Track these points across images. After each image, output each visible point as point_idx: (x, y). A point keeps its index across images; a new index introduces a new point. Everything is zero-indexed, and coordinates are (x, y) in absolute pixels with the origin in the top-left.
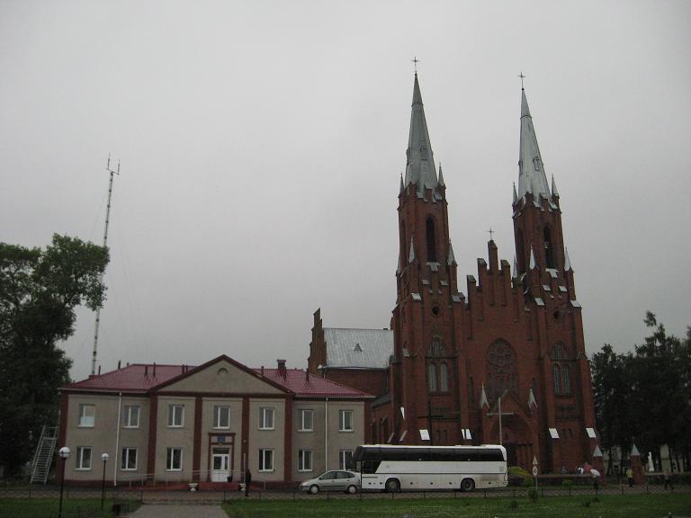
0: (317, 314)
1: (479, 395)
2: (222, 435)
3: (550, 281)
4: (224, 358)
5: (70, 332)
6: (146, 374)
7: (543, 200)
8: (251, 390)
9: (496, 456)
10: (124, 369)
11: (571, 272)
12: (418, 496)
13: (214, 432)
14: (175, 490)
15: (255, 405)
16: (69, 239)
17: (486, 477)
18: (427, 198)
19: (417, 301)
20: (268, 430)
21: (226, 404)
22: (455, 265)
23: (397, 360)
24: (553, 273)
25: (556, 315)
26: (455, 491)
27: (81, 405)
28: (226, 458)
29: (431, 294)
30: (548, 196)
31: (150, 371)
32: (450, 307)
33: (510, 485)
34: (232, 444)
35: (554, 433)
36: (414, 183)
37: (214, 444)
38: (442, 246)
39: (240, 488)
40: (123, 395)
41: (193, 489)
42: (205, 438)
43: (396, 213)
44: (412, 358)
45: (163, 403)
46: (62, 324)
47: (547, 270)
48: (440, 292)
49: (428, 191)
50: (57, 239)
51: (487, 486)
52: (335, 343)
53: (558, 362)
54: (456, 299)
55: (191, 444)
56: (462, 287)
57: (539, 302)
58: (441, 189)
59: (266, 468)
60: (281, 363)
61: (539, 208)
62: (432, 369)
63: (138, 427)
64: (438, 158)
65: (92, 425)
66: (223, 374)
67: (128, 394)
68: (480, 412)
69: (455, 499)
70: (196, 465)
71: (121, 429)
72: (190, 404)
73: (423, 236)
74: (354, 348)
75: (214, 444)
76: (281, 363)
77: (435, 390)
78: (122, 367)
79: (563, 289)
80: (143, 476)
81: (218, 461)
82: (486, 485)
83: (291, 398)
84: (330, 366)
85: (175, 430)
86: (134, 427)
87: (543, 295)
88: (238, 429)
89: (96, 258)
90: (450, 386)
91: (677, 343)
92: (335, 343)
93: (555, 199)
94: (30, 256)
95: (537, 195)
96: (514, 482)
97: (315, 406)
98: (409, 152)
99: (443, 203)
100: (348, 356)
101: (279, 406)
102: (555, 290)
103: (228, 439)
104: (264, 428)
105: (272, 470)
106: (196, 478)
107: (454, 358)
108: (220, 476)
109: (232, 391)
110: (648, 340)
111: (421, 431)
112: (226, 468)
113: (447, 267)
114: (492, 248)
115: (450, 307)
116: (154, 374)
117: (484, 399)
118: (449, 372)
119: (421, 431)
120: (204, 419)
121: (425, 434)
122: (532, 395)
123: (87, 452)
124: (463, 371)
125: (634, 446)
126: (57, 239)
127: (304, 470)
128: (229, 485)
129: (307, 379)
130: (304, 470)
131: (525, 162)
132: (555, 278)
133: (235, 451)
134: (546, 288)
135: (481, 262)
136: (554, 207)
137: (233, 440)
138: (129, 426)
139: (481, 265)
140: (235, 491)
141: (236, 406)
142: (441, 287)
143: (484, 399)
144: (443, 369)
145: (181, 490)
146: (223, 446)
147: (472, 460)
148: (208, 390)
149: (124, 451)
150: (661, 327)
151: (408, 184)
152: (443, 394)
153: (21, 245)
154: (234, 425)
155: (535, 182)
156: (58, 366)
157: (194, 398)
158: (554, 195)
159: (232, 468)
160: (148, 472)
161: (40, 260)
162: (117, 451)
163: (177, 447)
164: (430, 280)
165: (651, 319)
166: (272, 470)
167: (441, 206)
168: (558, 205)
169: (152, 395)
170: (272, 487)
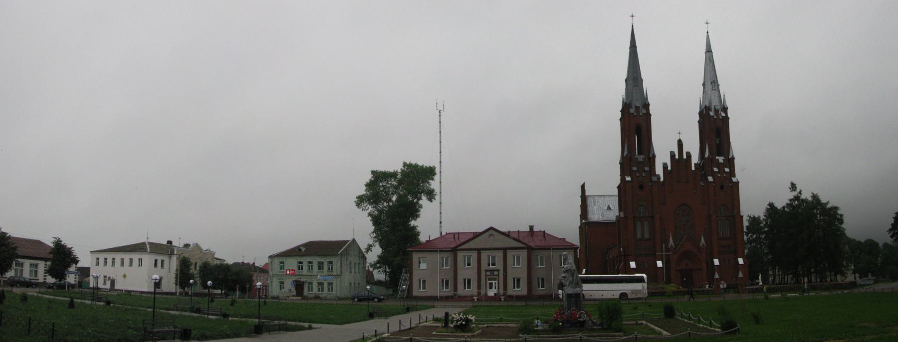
0: (583, 186)
2: (492, 271)
4: (491, 228)
5: (418, 216)
8: (507, 246)
9: (640, 280)
10: (444, 236)
11: (733, 158)
12: (592, 302)
14: (467, 301)
15: (510, 254)
16: (412, 164)
17: (634, 292)
18: (637, 113)
19: (628, 181)
20: (518, 268)
21: (494, 254)
22: (654, 156)
24: (721, 159)
25: (722, 187)
26: (645, 299)
27: (419, 258)
28: (495, 283)
29: (638, 176)
30: (718, 108)
31: (456, 236)
33: (648, 296)
34: (498, 275)
35: (716, 262)
36: (628, 103)
37: (488, 276)
39: (501, 299)
40: (440, 251)
41: (476, 300)
42: (483, 273)
43: (619, 122)
45: (460, 255)
46: (413, 211)
47: (717, 158)
49: (637, 108)
50: (405, 164)
51: (636, 297)
52: (594, 205)
53: (721, 218)
54: (654, 179)
55: (476, 276)
57: (710, 179)
58: (647, 106)
59: (517, 288)
60: (531, 228)
61: (713, 116)
64: (646, 85)
65: (425, 268)
66: (492, 237)
67: (442, 251)
69: (508, 305)
70: (479, 287)
71: (440, 269)
72: (474, 255)
74: (606, 208)
75: (488, 276)
76: (531, 228)
78: (443, 235)
79: (727, 170)
80: (452, 293)
81: (491, 284)
82: (634, 296)
83: (530, 249)
84: (591, 220)
85: (467, 272)
87: (713, 174)
89: (429, 173)
92: (594, 205)
93: (725, 109)
94: (393, 175)
96: (651, 294)
97: (546, 253)
98: (626, 81)
99: (648, 116)
100: (602, 213)
101: (524, 254)
102: (721, 170)
103: (496, 273)
104: (516, 266)
105: (520, 289)
106: (479, 294)
108: (491, 293)
112: (495, 288)
113: (649, 158)
115: (650, 184)
116: (458, 238)
120: (502, 259)
121: (633, 265)
122: (702, 238)
123: (424, 282)
125: (740, 272)
126: (405, 164)
127: (541, 289)
128: (496, 297)
130: (541, 289)
131: (706, 84)
132: (722, 163)
134: (716, 170)
136: (723, 115)
137: (486, 273)
138: (445, 268)
139: (672, 155)
140: (497, 301)
141: (499, 255)
142: (644, 171)
144: (646, 224)
145: (470, 301)
146: (493, 277)
147: (626, 283)
148: (484, 247)
149: (443, 281)
153: (386, 170)
154: (499, 265)
155: (713, 97)
156: (413, 234)
159: (499, 288)
160: (454, 291)
161: (399, 176)
162: (439, 280)
163: (469, 278)
165: (793, 187)
166: (520, 289)
169: (454, 250)
170: (519, 298)
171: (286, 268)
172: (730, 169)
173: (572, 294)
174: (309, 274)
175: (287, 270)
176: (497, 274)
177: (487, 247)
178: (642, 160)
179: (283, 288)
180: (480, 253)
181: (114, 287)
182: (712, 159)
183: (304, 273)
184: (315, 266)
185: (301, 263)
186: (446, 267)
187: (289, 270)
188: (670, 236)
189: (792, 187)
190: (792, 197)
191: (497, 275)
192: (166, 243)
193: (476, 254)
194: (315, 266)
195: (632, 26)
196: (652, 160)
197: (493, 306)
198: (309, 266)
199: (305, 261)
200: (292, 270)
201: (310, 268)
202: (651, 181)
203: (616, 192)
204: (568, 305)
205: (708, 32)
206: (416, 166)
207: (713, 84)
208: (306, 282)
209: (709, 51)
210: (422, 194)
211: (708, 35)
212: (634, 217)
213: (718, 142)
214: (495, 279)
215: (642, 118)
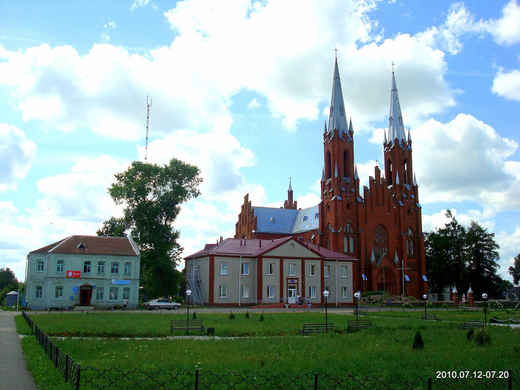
0: (246, 197)
1: (370, 255)
2: (292, 279)
6: (241, 244)
13: (289, 277)
24: (408, 187)
25: (409, 211)
28: (294, 291)
34: (297, 283)
40: (243, 257)
42: (285, 281)
45: (266, 263)
48: (351, 196)
54: (360, 200)
56: (361, 193)
63: (248, 274)
72: (277, 262)
81: (291, 292)
86: (247, 274)
88: (299, 276)
90: (354, 249)
91: (463, 229)
95: (400, 140)
101: (318, 263)
103: (296, 281)
109: (297, 256)
110: (447, 225)
112: (294, 296)
116: (245, 245)
117: (373, 258)
118: (354, 242)
124: (363, 242)
129: (319, 249)
142: (351, 192)
143: (373, 258)
144: (351, 239)
151: (331, 129)
157: (279, 259)
163: (345, 286)
164: (346, 188)
171: (65, 270)
174: (98, 277)
175: (68, 272)
177: (288, 256)
179: (61, 295)
180: (304, 261)
181: (319, 304)
183: (92, 277)
184: (108, 268)
185: (116, 264)
186: (245, 273)
187: (72, 272)
191: (296, 283)
192: (96, 235)
193: (352, 265)
194: (108, 268)
196: (356, 182)
198: (99, 268)
199: (94, 261)
200: (76, 272)
201: (101, 270)
206: (498, 192)
207: (400, 119)
208: (95, 286)
210: (123, 184)
214: (294, 288)
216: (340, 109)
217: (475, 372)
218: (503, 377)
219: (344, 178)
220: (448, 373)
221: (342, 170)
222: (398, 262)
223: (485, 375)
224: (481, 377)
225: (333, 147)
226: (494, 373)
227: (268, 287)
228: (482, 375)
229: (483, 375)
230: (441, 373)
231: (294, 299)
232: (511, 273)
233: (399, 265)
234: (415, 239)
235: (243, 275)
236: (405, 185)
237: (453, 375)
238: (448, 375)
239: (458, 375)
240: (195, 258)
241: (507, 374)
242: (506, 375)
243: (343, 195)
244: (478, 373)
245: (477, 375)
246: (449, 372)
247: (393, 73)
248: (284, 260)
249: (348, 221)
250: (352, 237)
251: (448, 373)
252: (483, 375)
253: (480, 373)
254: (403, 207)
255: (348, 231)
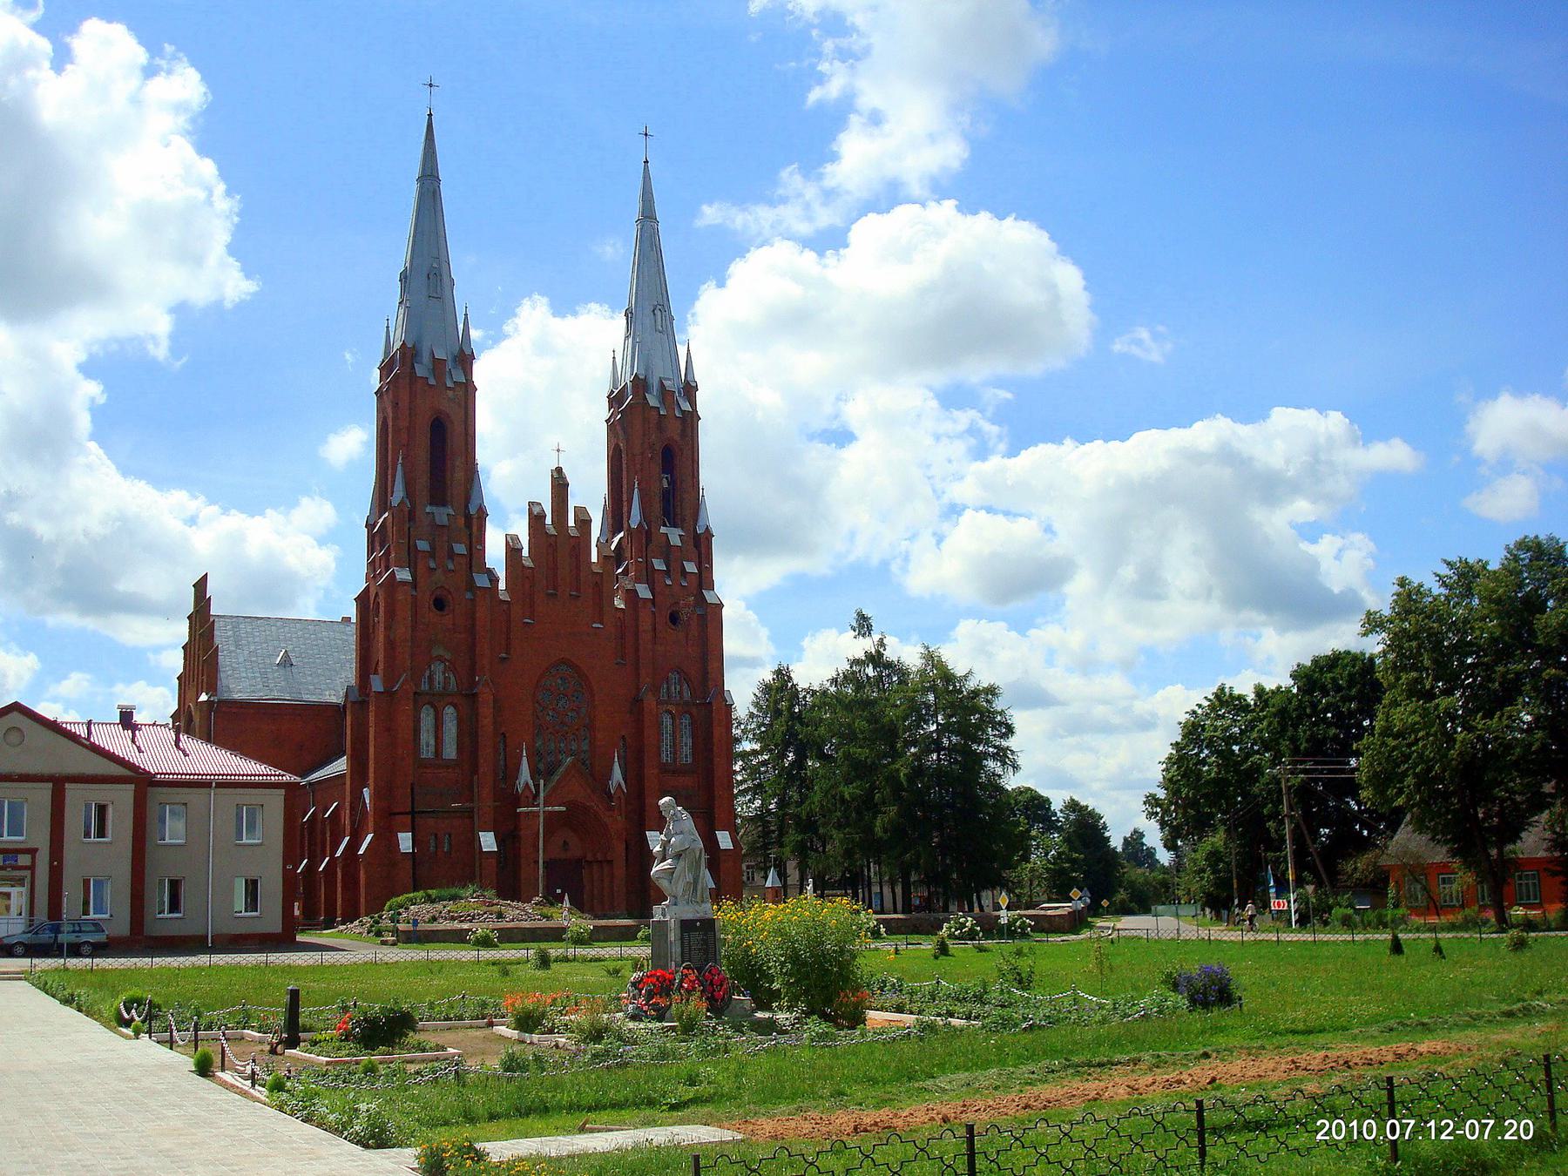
0: (201, 586)
3: (667, 551)
7: (665, 393)
11: (708, 534)
19: (404, 583)
22: (482, 514)
23: (360, 695)
24: (675, 536)
25: (674, 618)
32: (469, 595)
34: (32, 868)
38: (459, 475)
43: (415, 186)
44: (388, 693)
48: (451, 566)
49: (438, 364)
53: (670, 707)
54: (482, 581)
62: (887, 890)
66: (14, 737)
68: (516, 800)
73: (422, 454)
77: (430, 755)
84: (225, 696)
88: (42, 841)
90: (460, 749)
98: (404, 278)
99: (690, 421)
103: (24, 860)
107: (473, 697)
111: (400, 835)
113: (468, 517)
114: (560, 485)
118: (460, 722)
119: (400, 835)
124: (487, 721)
133: (37, 883)
134: (659, 565)
135: (536, 510)
136: (686, 407)
137: (33, 859)
139: (536, 519)
142: (451, 555)
144: (449, 711)
150: (881, 643)
152: (448, 765)
158: (687, 383)
167: (461, 393)
168: (693, 403)
172: (699, 567)
173: (693, 921)
176: (29, 864)
178: (445, 521)
182: (648, 534)
188: (522, 756)
189: (861, 626)
190: (861, 655)
191: (25, 868)
195: (430, 115)
197: (584, 960)
202: (471, 585)
203: (352, 611)
204: (682, 952)
205: (646, 162)
207: (658, 313)
209: (429, 179)
211: (646, 170)
212: (415, 693)
213: (666, 485)
214: (20, 882)
215: (450, 393)
216: (429, 278)
217: (1432, 1123)
218: (1516, 1138)
219: (428, 509)
220: (1351, 1125)
221: (423, 480)
222: (619, 784)
223: (1462, 1132)
224: (1452, 1138)
225: (396, 405)
226: (1488, 1124)
227: (86, 883)
228: (1454, 1130)
229: (1458, 1132)
230: (1331, 1126)
231: (19, 921)
232: (1153, 814)
233: (622, 796)
234: (694, 711)
235: (240, 845)
236: (663, 530)
237: (1474, 1131)
238: (1350, 1131)
239: (1381, 1129)
240: (220, 785)
241: (1474, 1128)
242: (1527, 1132)
243: (420, 566)
244: (1443, 1124)
245: (1439, 1131)
246: (1355, 1123)
247: (646, 162)
248: (67, 785)
249: (438, 651)
250: (455, 706)
251: (1351, 1125)
252: (1458, 1132)
253: (1448, 1125)
254: (650, 604)
255: (438, 686)
